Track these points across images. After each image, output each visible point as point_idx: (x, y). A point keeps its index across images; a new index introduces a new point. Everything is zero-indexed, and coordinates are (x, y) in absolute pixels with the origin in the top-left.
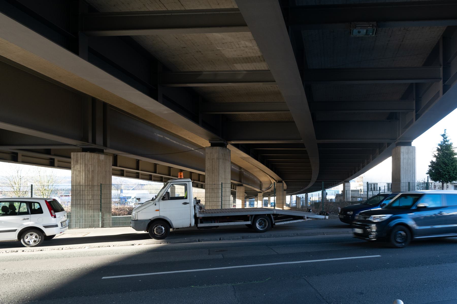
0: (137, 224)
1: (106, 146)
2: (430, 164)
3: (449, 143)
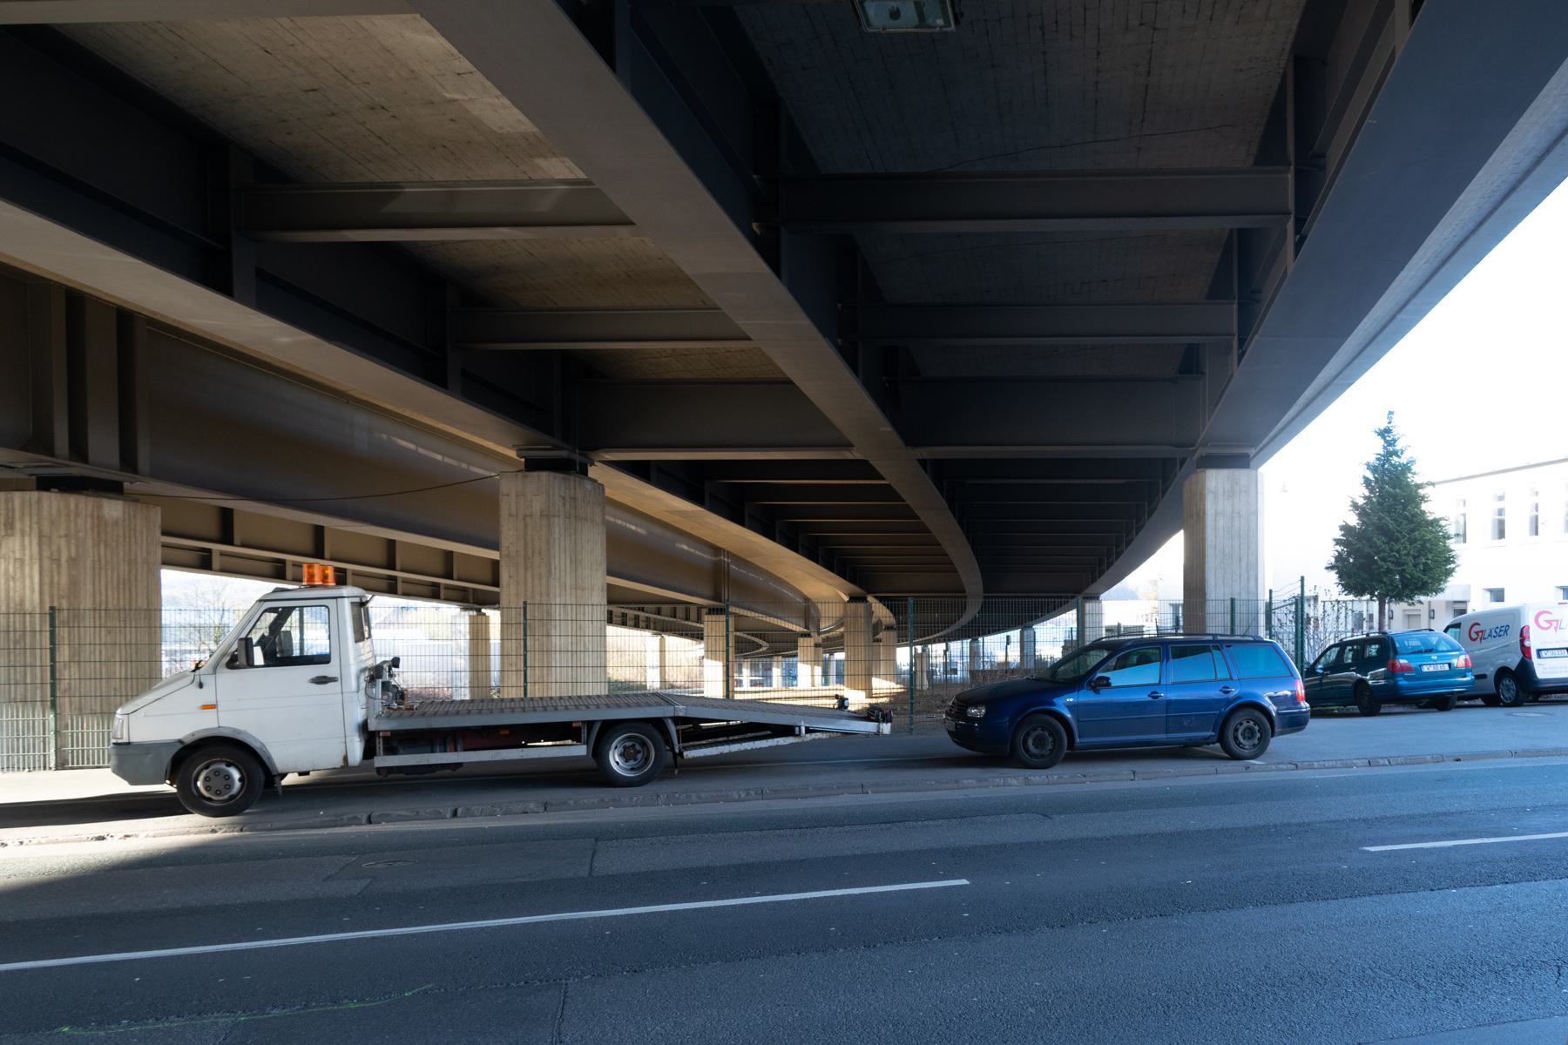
0: (128, 758)
1: (135, 470)
2: (1338, 534)
3: (1404, 460)
